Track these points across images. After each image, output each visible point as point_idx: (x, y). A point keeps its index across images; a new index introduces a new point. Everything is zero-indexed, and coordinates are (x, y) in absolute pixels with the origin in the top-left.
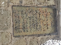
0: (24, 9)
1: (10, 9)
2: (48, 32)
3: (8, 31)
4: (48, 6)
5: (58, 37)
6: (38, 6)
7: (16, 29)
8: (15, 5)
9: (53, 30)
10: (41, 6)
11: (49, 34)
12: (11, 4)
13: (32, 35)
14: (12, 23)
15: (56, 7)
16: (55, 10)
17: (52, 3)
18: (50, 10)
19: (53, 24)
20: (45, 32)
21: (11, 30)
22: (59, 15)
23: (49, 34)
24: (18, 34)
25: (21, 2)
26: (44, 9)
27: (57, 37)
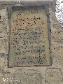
0: (12, 51)
1: (12, 70)
2: (44, 18)
3: (43, 73)
4: (9, 18)
5: (52, 4)
6: (8, 31)
7: (40, 62)
8: (6, 64)
9: (42, 11)
10: (8, 27)
11: (48, 16)
12: (6, 69)
13: (50, 41)
14: (32, 68)
15: (10, 7)
16: (14, 8)
17: (4, 13)
18: (15, 15)
19: (33, 11)
20: (45, 22)
21: (42, 69)
22: (21, 3)
23: (48, 16)
24: (48, 60)
25: (3, 55)
26: (12, 24)
27: (51, 6)
